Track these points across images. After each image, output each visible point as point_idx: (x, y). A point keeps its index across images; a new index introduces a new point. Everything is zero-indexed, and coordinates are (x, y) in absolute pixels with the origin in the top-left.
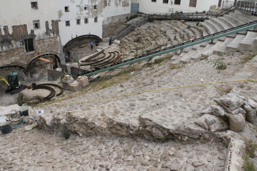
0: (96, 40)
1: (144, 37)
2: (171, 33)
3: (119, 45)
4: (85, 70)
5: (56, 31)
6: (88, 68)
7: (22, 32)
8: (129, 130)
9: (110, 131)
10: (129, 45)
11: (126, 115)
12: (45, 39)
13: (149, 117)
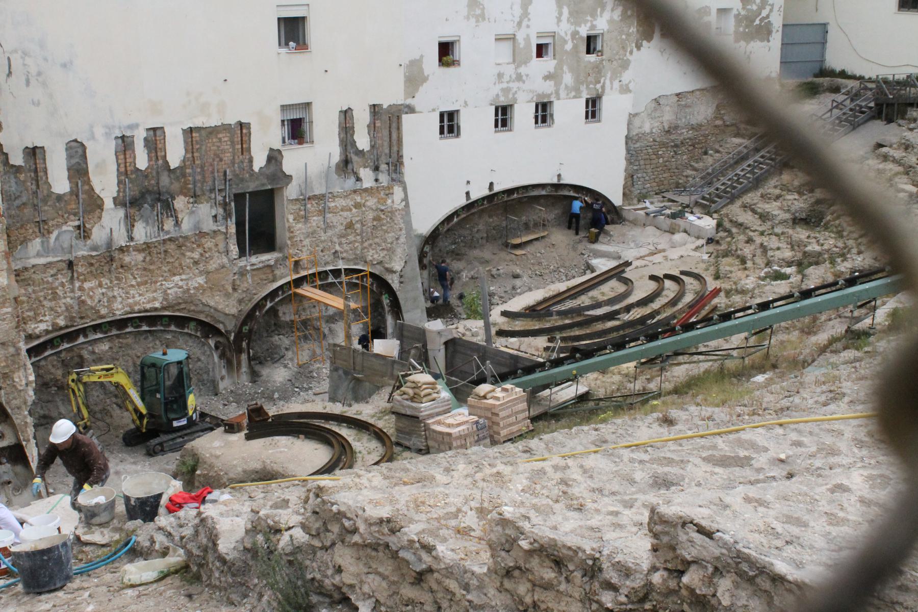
0: (588, 214)
3: (710, 241)
4: (515, 358)
5: (389, 158)
6: (534, 348)
7: (227, 157)
8: (596, 585)
9: (507, 590)
10: (765, 239)
11: (597, 511)
12: (334, 197)
13: (701, 515)
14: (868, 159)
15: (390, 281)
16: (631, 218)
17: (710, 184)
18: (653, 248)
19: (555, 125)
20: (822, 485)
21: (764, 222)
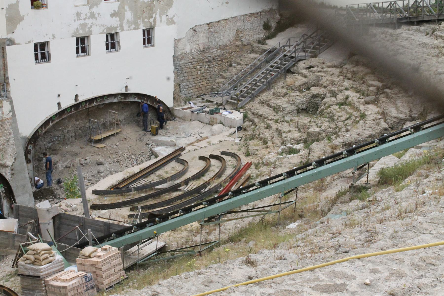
0: (148, 113)
1: (334, 94)
3: (240, 129)
6: (121, 216)
10: (279, 125)
14: (345, 64)
15: (4, 174)
16: (181, 116)
19: (121, 50)
21: (277, 113)
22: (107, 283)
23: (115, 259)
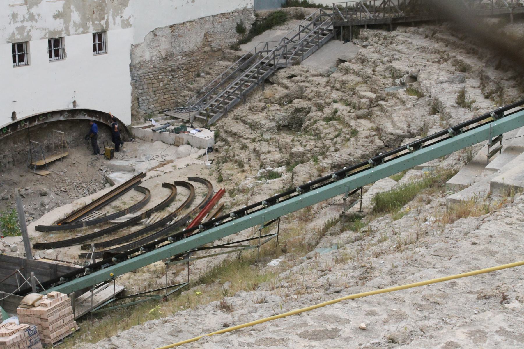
0: (99, 133)
1: (320, 108)
2: (441, 78)
3: (210, 150)
4: (55, 268)
6: (70, 256)
10: (257, 145)
16: (140, 136)
17: (204, 101)
18: (162, 160)
19: (67, 58)
20: (436, 345)
21: (254, 130)
22: (55, 336)
23: (64, 308)
